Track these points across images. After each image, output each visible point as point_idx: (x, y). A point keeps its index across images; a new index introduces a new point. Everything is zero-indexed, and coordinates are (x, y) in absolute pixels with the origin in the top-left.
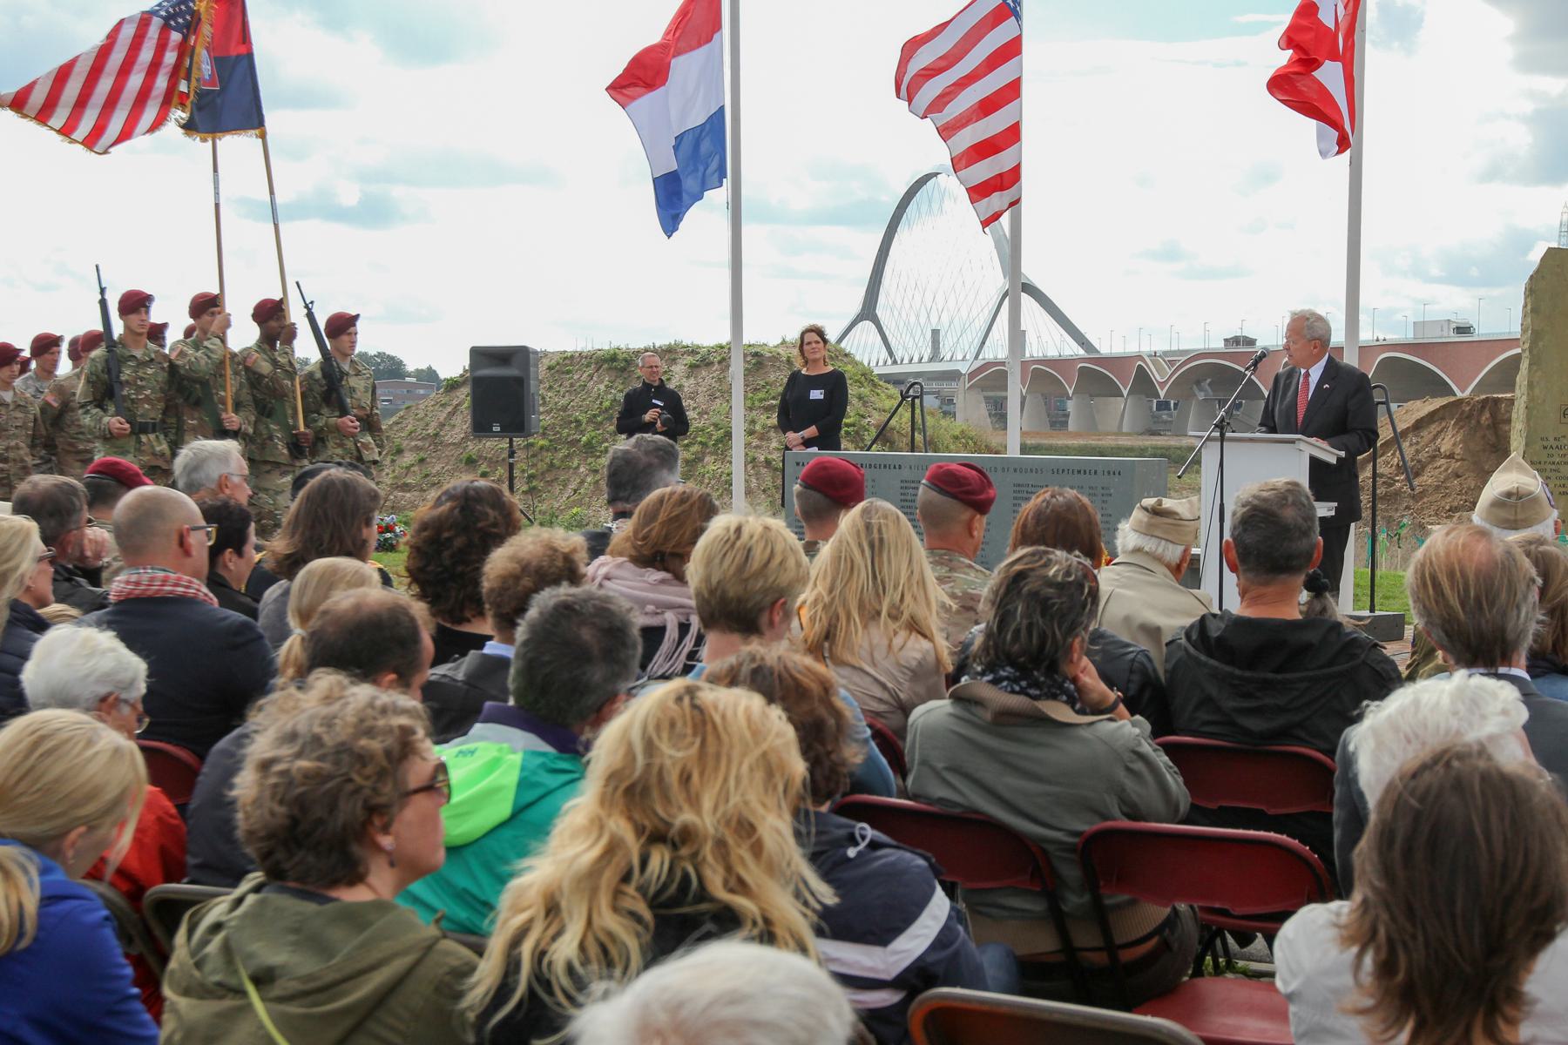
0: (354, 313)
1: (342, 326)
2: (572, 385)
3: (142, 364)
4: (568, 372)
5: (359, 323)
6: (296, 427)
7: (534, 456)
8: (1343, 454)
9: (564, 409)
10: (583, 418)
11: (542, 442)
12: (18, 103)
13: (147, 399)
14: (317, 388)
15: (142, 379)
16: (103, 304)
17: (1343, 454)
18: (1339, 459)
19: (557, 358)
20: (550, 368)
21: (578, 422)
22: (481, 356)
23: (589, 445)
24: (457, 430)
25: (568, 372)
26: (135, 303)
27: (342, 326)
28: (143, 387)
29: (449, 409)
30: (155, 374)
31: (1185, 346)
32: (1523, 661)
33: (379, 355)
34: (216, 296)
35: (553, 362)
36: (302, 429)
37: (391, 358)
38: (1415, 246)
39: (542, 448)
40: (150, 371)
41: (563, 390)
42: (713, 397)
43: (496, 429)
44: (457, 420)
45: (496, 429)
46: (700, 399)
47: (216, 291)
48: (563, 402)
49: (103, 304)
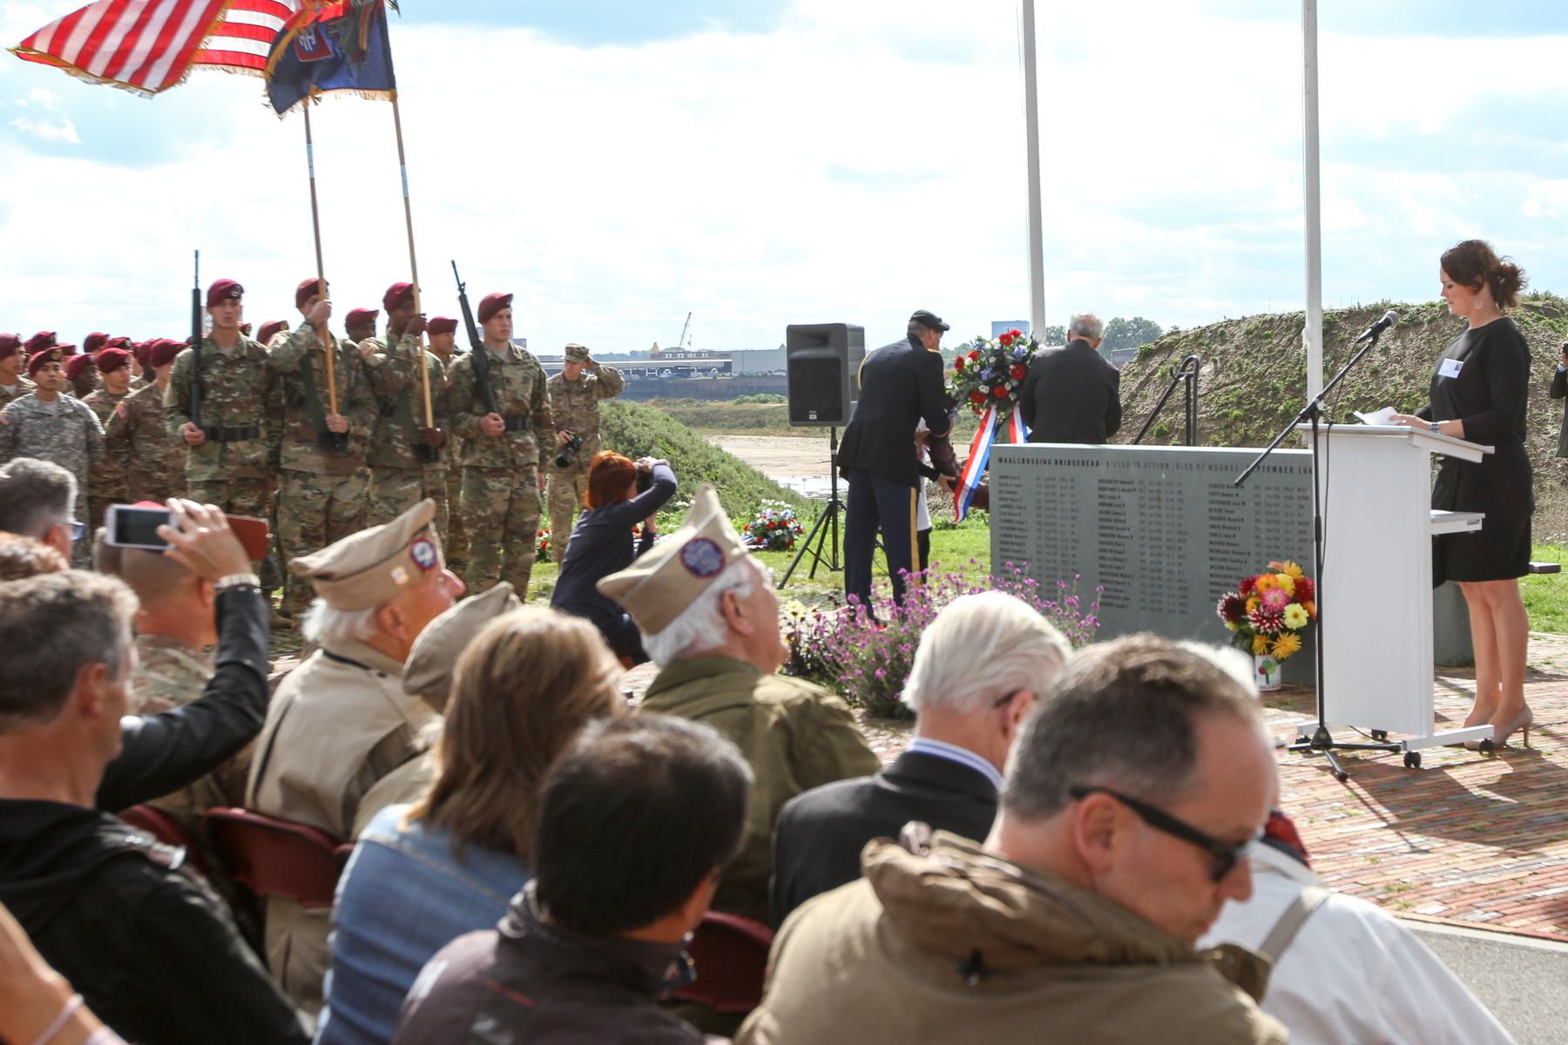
0: (505, 292)
1: (496, 307)
2: (1270, 350)
3: (231, 363)
4: (1267, 337)
5: (513, 304)
6: (424, 422)
7: (1228, 427)
8: (1491, 449)
9: (1262, 376)
10: (1281, 385)
11: (1236, 412)
12: (25, 50)
13: (236, 403)
14: (465, 382)
15: (229, 380)
16: (197, 293)
17: (1491, 449)
18: (1486, 456)
19: (1255, 322)
20: (1248, 333)
21: (1276, 390)
22: (799, 335)
23: (1286, 412)
24: (1149, 401)
25: (1267, 337)
26: (226, 294)
27: (496, 307)
28: (230, 390)
29: (1142, 378)
30: (245, 374)
31: (421, 295)
32: (168, 849)
33: (1136, 321)
34: (411, 286)
35: (1252, 327)
36: (430, 424)
37: (1149, 324)
38: (341, 1)
39: (1236, 418)
40: (239, 371)
41: (1260, 356)
42: (1421, 360)
43: (813, 417)
44: (1149, 390)
45: (813, 417)
46: (1407, 362)
47: (409, 281)
48: (1260, 369)
49: (197, 293)
